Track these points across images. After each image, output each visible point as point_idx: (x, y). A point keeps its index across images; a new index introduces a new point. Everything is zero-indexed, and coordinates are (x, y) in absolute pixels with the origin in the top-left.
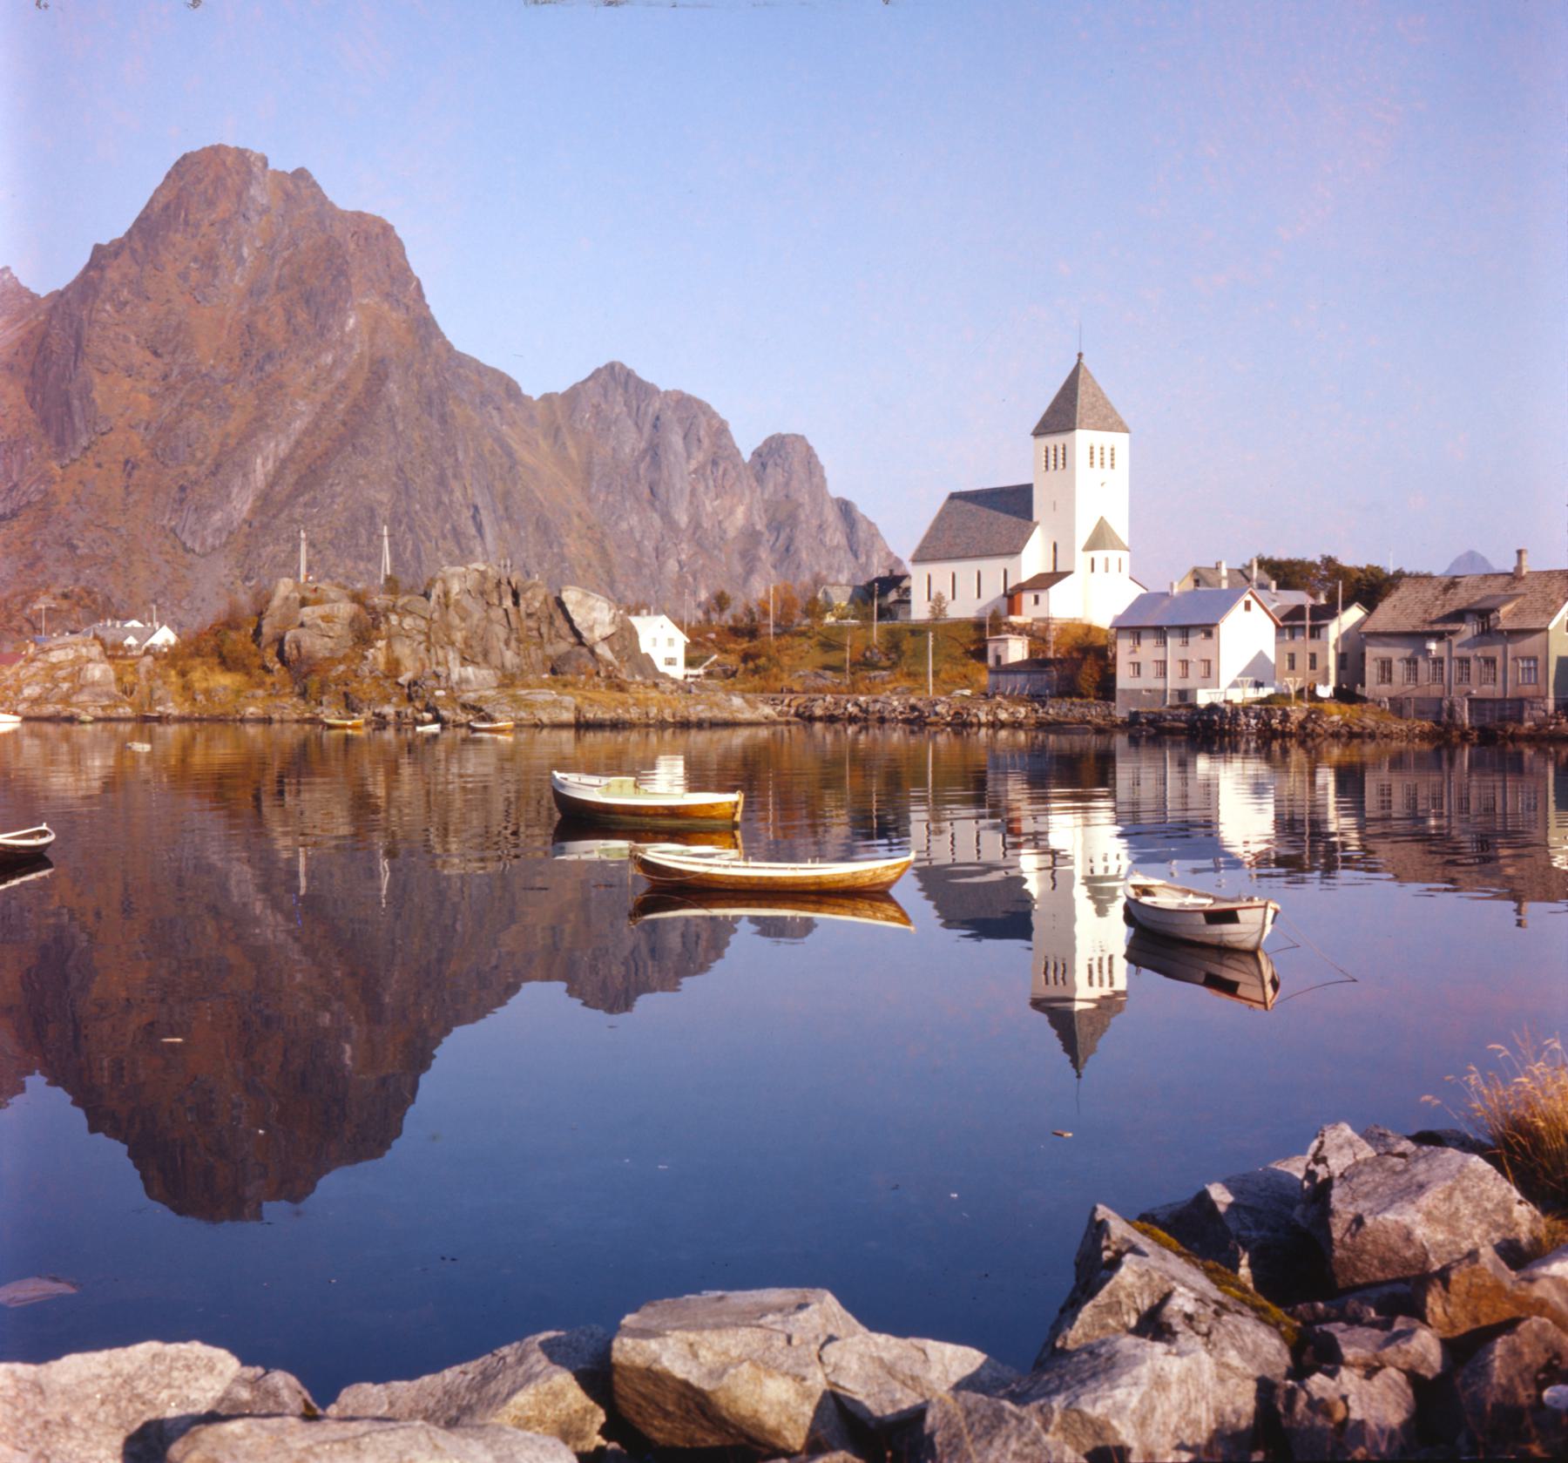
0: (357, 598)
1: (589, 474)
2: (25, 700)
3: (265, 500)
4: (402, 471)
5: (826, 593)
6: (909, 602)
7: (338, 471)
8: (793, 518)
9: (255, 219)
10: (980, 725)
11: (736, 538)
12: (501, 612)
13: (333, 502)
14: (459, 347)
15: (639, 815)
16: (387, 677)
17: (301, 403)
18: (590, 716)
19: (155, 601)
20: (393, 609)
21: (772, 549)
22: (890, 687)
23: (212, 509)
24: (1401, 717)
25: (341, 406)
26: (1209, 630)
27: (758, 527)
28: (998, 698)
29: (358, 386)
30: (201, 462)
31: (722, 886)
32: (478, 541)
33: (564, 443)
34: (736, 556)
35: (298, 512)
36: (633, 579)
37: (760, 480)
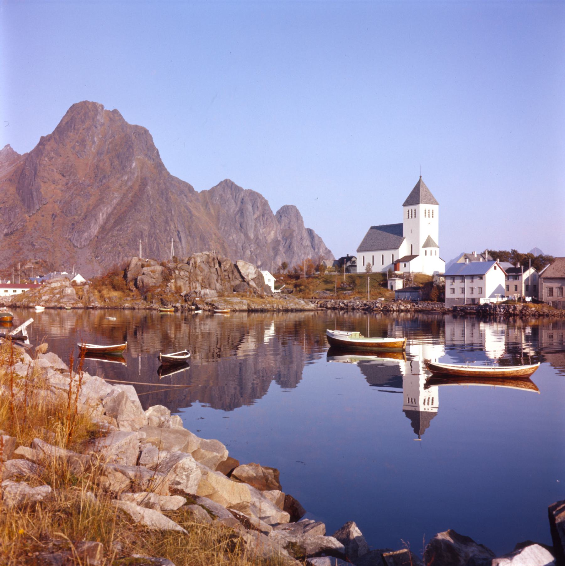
0: (162, 264)
1: (218, 219)
2: (43, 301)
3: (103, 228)
4: (152, 218)
5: (324, 263)
6: (356, 266)
7: (130, 218)
8: (291, 235)
9: (99, 127)
10: (394, 311)
11: (271, 243)
12: (215, 269)
13: (128, 229)
14: (173, 173)
15: (366, 346)
16: (176, 293)
17: (116, 194)
18: (253, 307)
19: (63, 265)
20: (176, 268)
21: (284, 247)
22: (352, 297)
23: (84, 232)
24: (557, 309)
25: (130, 195)
26: (481, 277)
27: (279, 239)
28: (400, 301)
29: (136, 187)
30: (80, 215)
31: (464, 375)
32: (179, 244)
33: (209, 208)
34: (271, 249)
35: (115, 233)
36: (234, 257)
37: (279, 222)
